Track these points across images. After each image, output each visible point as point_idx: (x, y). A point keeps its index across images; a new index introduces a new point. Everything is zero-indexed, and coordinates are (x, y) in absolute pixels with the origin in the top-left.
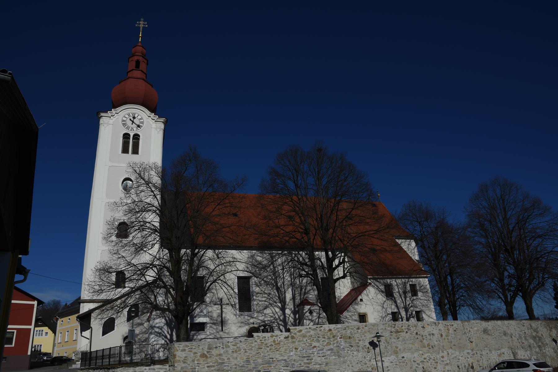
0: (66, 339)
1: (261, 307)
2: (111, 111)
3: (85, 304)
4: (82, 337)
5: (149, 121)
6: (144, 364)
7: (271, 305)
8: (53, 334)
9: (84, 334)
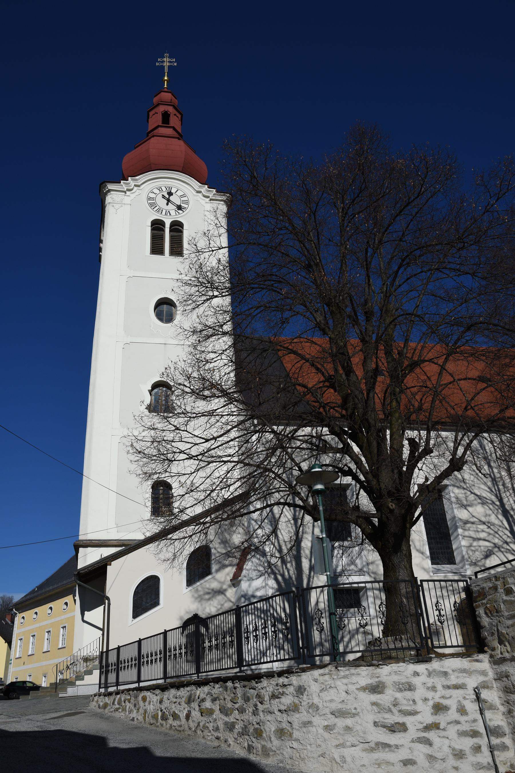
0: (30, 649)
1: (477, 553)
2: (127, 180)
3: (89, 549)
4: (85, 624)
5: (199, 199)
6: (394, 654)
7: (499, 548)
8: (6, 644)
9: (89, 616)
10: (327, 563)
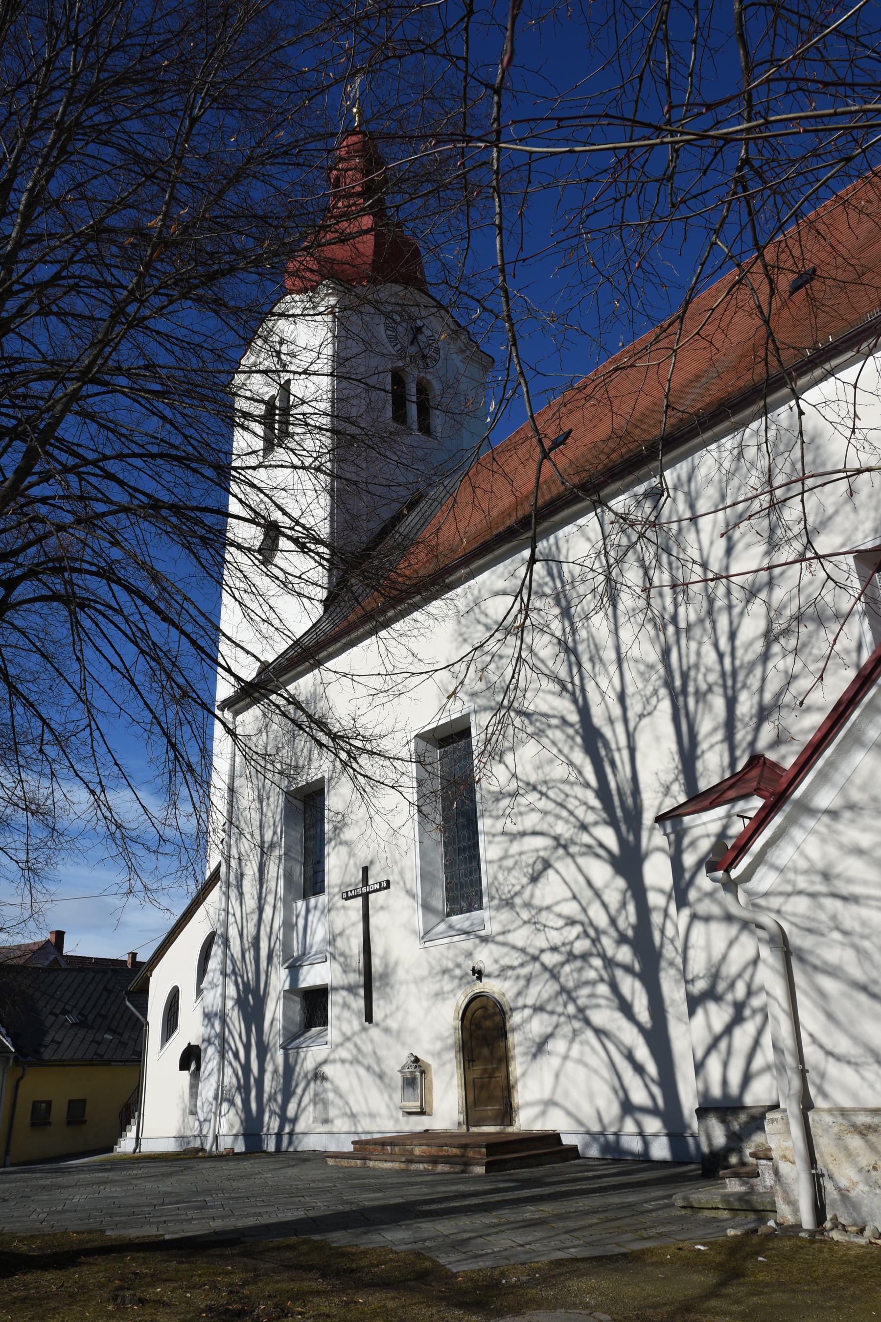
7: (565, 847)
10: (564, 1188)
